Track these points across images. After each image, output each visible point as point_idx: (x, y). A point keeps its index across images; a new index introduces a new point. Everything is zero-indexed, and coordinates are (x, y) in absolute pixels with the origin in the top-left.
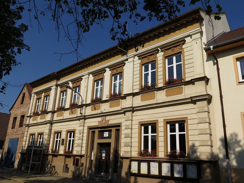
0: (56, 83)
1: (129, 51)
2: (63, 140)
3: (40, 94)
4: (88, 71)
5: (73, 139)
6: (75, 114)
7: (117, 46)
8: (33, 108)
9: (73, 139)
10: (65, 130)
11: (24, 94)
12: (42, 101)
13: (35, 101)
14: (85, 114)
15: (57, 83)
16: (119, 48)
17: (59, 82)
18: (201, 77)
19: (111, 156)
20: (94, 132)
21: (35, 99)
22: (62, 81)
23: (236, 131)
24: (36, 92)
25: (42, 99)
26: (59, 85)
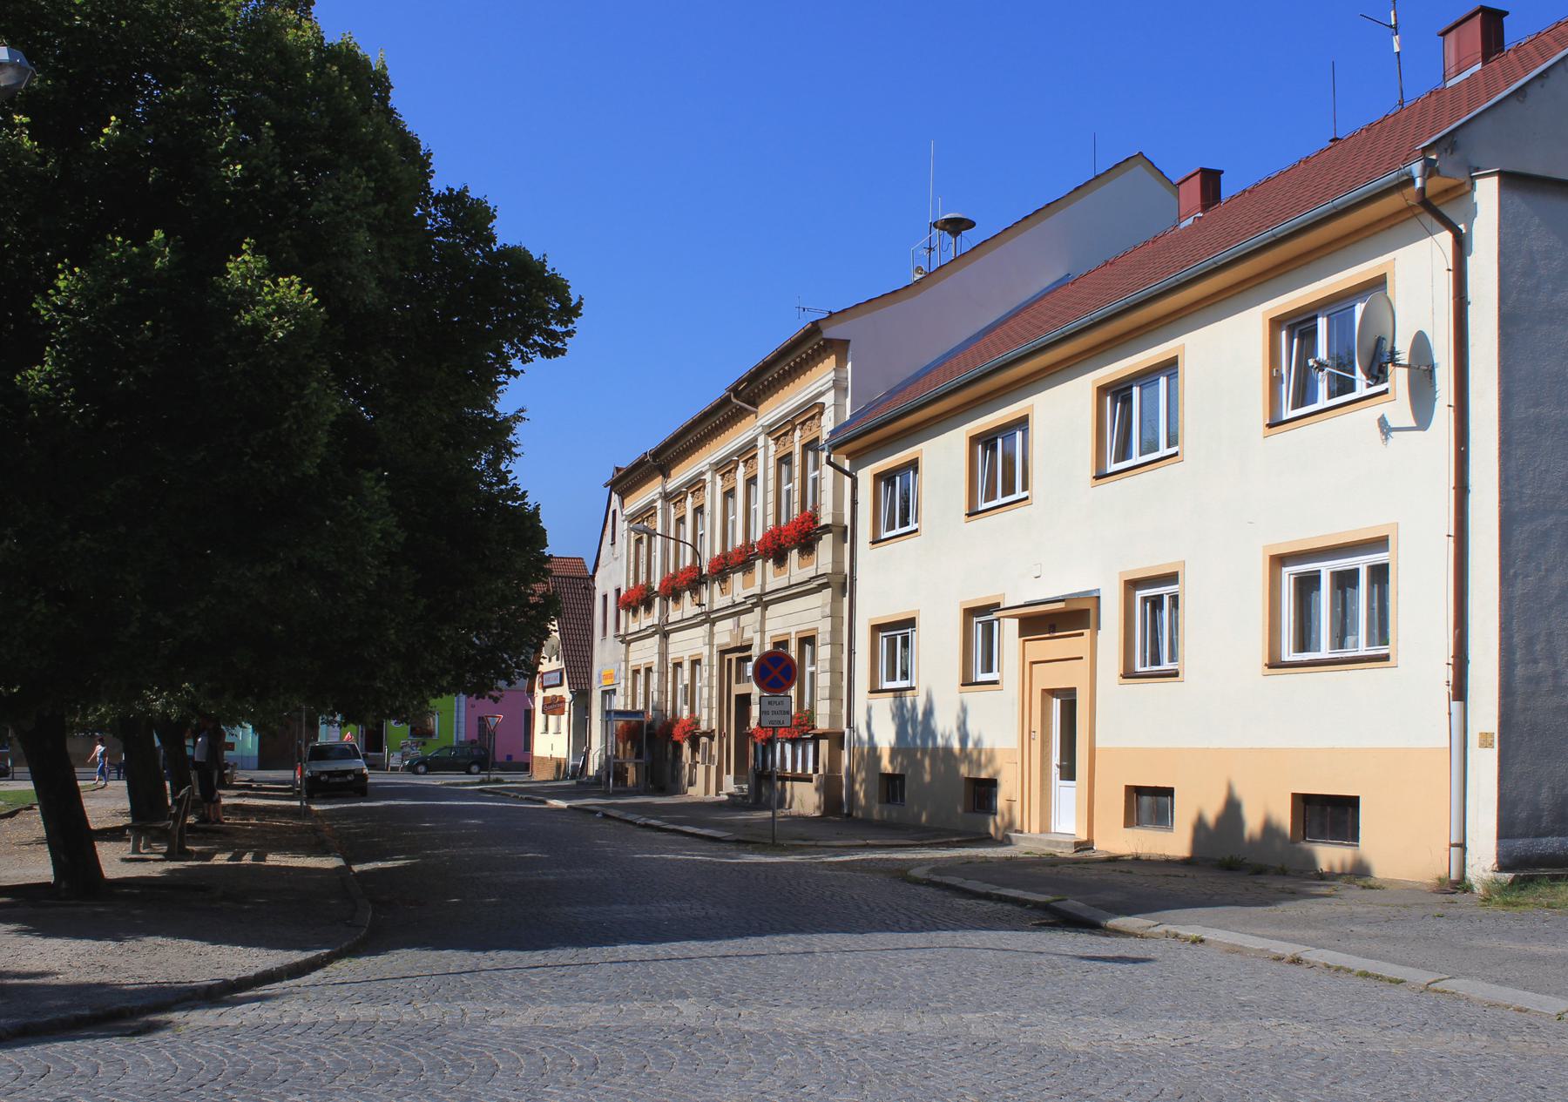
0: (660, 489)
1: (760, 407)
2: (686, 686)
3: (812, 418)
4: (708, 461)
5: (813, 668)
6: (786, 573)
7: (729, 397)
8: (771, 508)
9: (813, 668)
10: (686, 658)
11: (614, 512)
12: (797, 472)
13: (772, 473)
14: (711, 606)
15: (664, 488)
16: (734, 400)
17: (672, 484)
18: (1270, 342)
19: (668, 712)
20: (1307, 584)
21: (772, 462)
22: (681, 475)
23: (517, 685)
24: (717, 463)
25: (797, 459)
26: (671, 493)
